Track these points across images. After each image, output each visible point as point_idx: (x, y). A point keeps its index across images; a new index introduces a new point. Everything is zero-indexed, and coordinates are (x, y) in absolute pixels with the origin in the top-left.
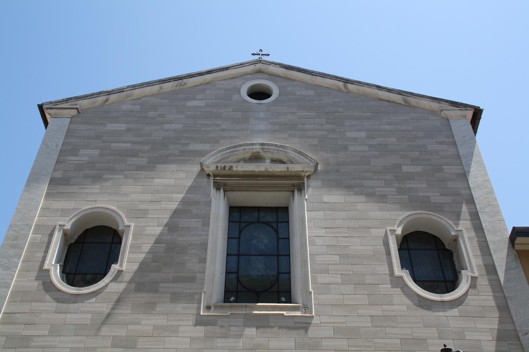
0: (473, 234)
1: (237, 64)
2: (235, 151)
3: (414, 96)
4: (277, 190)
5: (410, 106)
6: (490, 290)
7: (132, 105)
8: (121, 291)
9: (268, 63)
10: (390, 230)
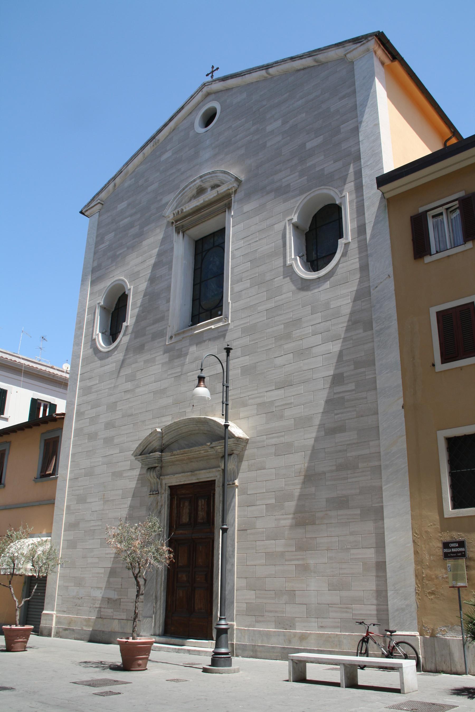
0: (354, 196)
2: (184, 193)
3: (322, 52)
4: (215, 215)
5: (322, 64)
7: (130, 180)
8: (128, 341)
9: (210, 83)
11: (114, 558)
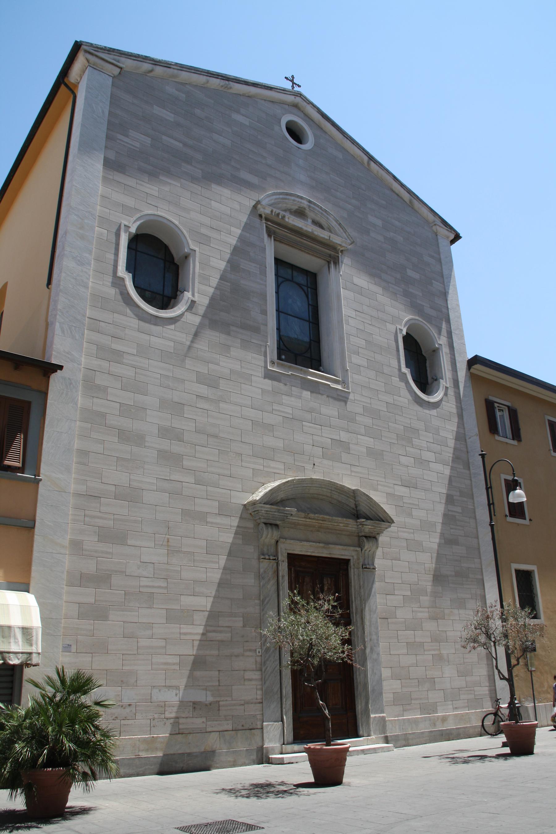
1: (281, 88)
3: (418, 200)
4: (317, 255)
6: (454, 400)
7: (176, 90)
10: (125, 225)
11: (200, 640)
